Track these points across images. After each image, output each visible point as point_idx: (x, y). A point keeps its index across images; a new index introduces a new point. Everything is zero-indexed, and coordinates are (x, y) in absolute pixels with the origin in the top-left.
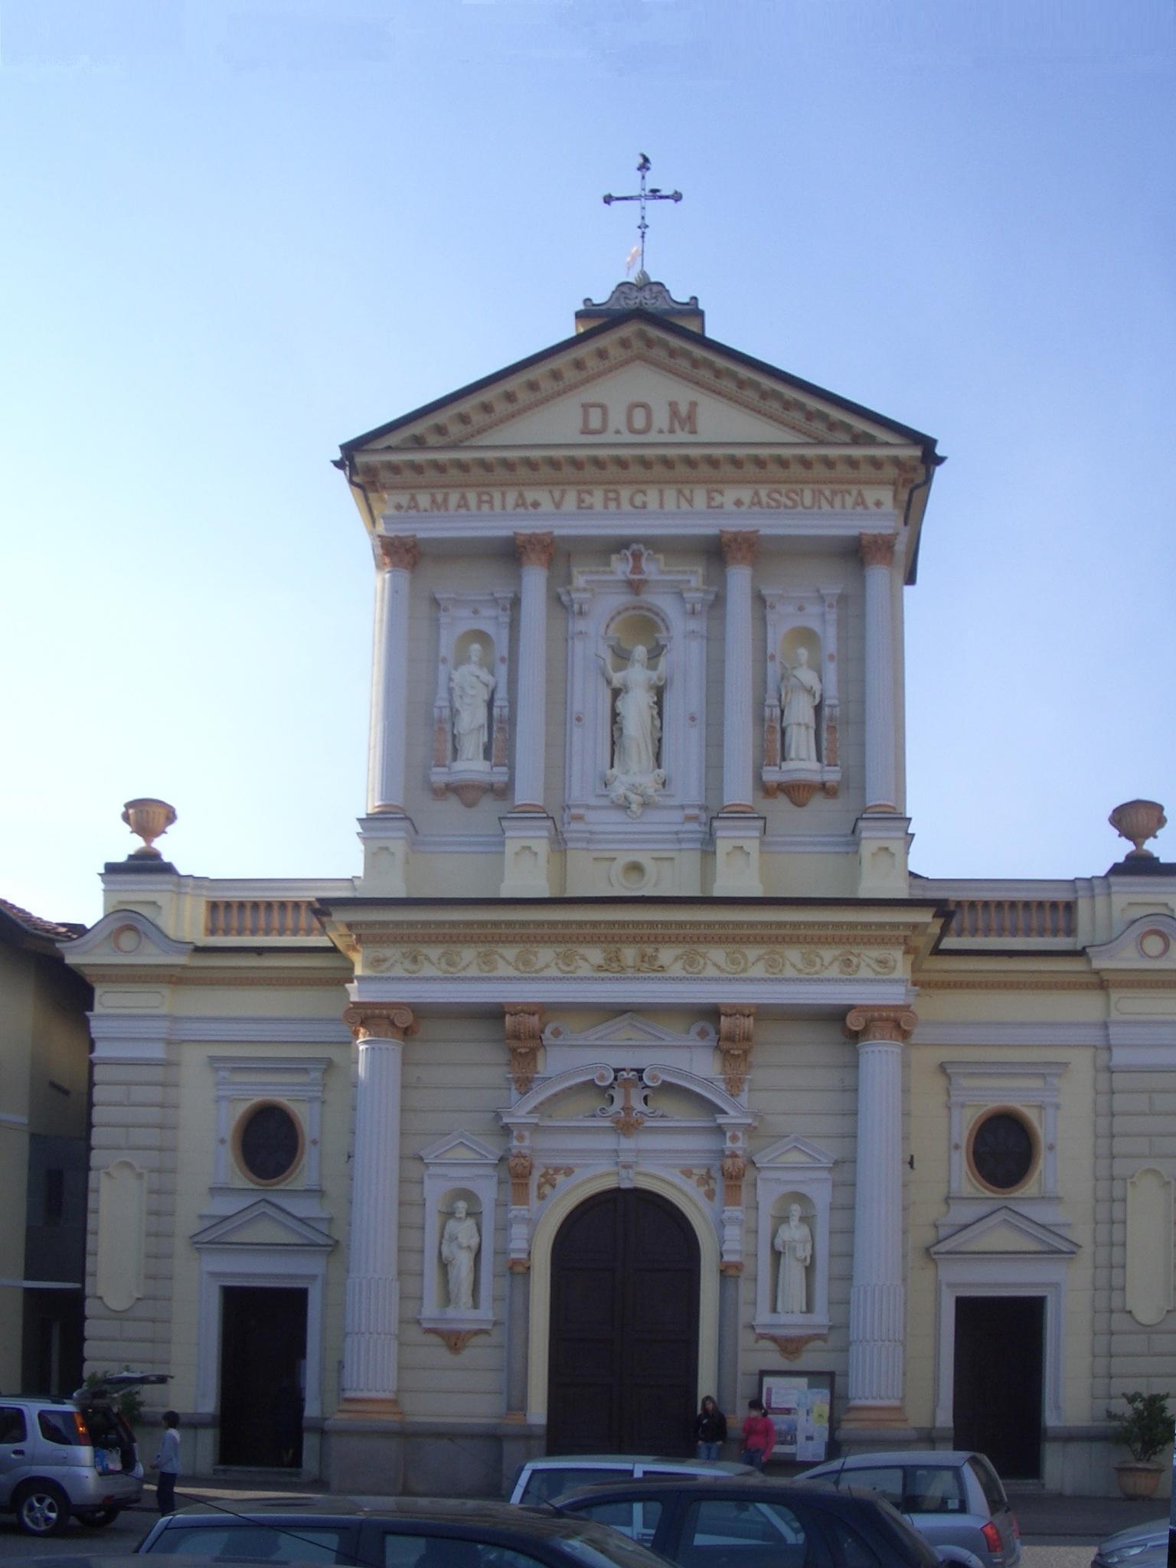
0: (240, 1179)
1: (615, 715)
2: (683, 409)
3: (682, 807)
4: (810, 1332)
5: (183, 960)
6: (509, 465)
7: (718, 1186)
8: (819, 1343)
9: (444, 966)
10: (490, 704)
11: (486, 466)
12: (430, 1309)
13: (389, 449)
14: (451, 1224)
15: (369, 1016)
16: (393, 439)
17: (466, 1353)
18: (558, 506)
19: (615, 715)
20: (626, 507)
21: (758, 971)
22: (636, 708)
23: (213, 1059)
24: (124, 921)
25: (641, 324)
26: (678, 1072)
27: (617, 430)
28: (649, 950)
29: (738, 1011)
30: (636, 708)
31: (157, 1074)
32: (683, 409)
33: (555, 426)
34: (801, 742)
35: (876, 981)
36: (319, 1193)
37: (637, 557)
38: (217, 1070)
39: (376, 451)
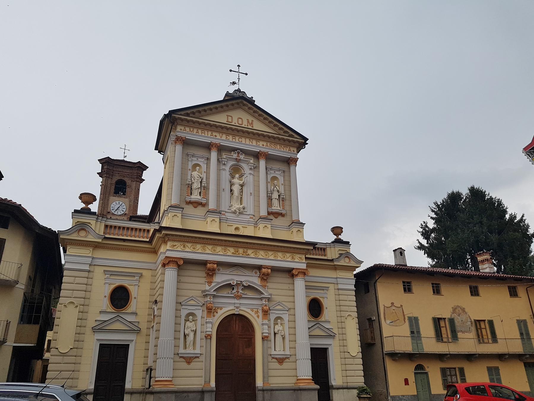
0: (110, 309)
1: (231, 190)
2: (250, 122)
3: (249, 215)
4: (284, 357)
5: (100, 240)
6: (211, 126)
7: (260, 314)
8: (288, 360)
9: (192, 249)
10: (201, 182)
11: (206, 125)
12: (181, 350)
13: (181, 115)
14: (188, 323)
15: (169, 262)
16: (182, 113)
17: (192, 364)
18: (221, 137)
19: (231, 190)
20: (237, 141)
21: (272, 257)
22: (236, 188)
23: (104, 271)
24: (79, 227)
25: (237, 100)
26: (252, 282)
27: (235, 122)
28: (245, 250)
29: (267, 267)
30: (236, 188)
31: (86, 274)
32: (250, 122)
33: (221, 118)
34: (275, 203)
35: (298, 263)
36: (135, 314)
37: (238, 153)
38: (105, 274)
39: (178, 115)
